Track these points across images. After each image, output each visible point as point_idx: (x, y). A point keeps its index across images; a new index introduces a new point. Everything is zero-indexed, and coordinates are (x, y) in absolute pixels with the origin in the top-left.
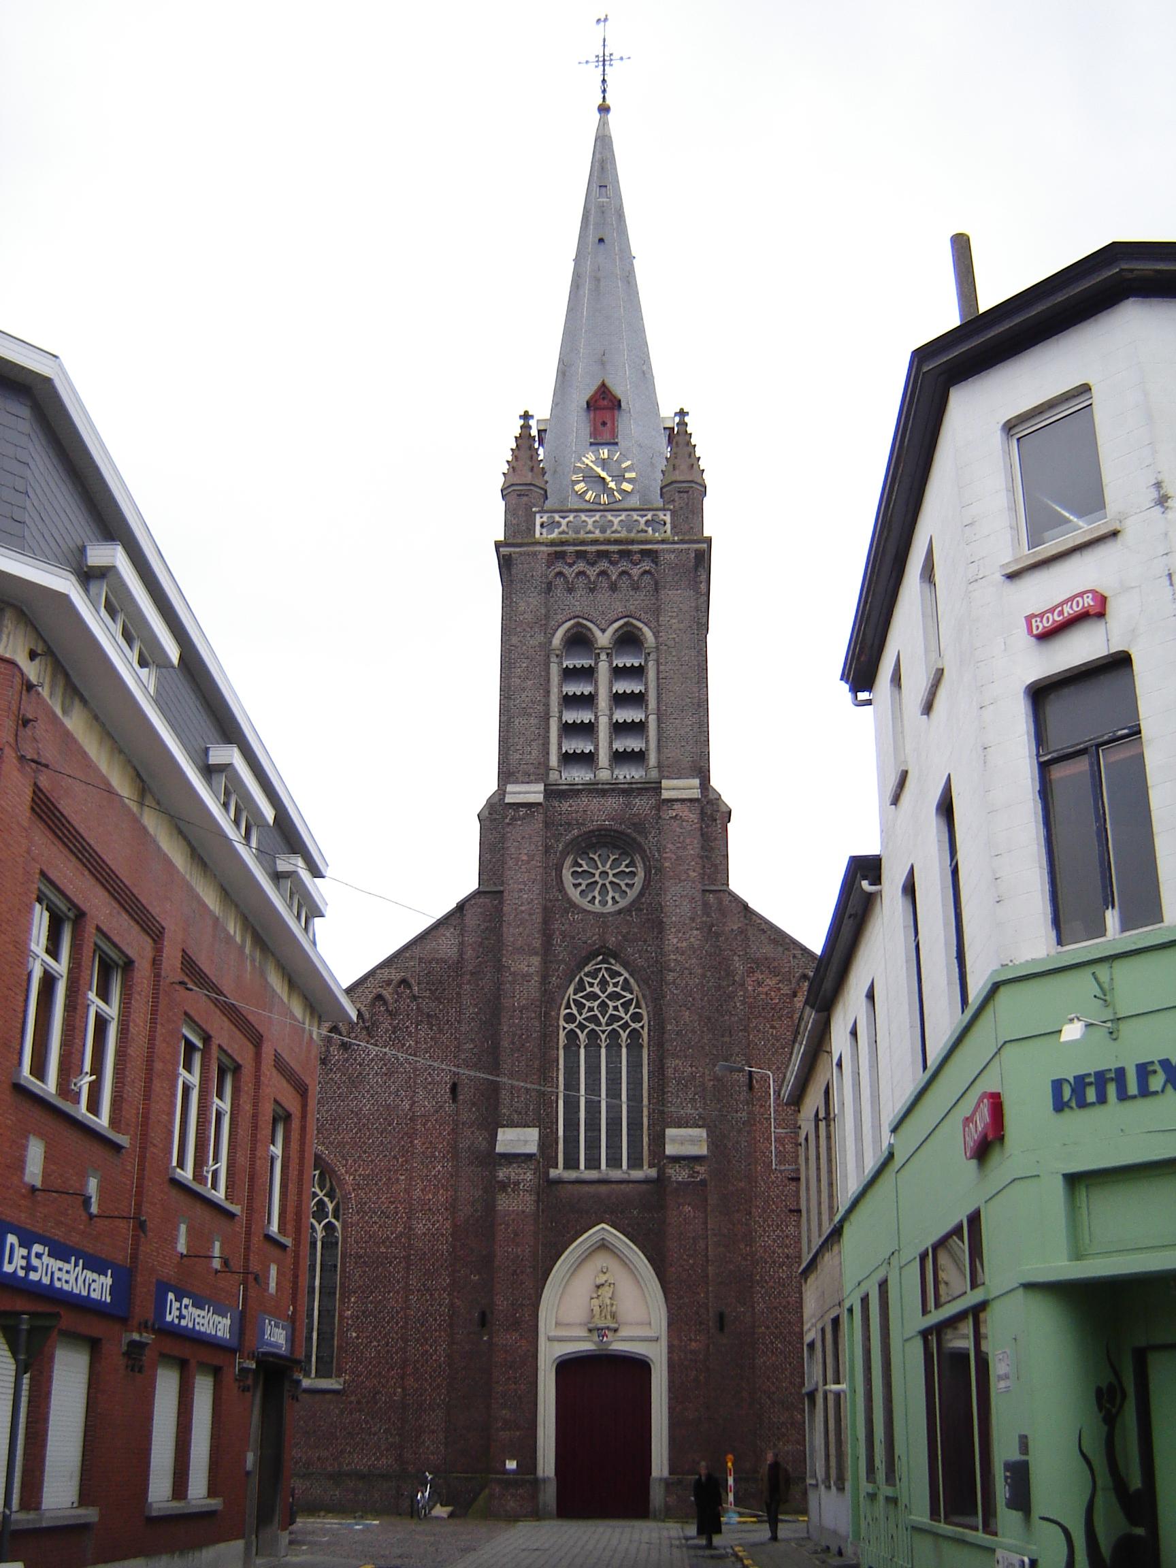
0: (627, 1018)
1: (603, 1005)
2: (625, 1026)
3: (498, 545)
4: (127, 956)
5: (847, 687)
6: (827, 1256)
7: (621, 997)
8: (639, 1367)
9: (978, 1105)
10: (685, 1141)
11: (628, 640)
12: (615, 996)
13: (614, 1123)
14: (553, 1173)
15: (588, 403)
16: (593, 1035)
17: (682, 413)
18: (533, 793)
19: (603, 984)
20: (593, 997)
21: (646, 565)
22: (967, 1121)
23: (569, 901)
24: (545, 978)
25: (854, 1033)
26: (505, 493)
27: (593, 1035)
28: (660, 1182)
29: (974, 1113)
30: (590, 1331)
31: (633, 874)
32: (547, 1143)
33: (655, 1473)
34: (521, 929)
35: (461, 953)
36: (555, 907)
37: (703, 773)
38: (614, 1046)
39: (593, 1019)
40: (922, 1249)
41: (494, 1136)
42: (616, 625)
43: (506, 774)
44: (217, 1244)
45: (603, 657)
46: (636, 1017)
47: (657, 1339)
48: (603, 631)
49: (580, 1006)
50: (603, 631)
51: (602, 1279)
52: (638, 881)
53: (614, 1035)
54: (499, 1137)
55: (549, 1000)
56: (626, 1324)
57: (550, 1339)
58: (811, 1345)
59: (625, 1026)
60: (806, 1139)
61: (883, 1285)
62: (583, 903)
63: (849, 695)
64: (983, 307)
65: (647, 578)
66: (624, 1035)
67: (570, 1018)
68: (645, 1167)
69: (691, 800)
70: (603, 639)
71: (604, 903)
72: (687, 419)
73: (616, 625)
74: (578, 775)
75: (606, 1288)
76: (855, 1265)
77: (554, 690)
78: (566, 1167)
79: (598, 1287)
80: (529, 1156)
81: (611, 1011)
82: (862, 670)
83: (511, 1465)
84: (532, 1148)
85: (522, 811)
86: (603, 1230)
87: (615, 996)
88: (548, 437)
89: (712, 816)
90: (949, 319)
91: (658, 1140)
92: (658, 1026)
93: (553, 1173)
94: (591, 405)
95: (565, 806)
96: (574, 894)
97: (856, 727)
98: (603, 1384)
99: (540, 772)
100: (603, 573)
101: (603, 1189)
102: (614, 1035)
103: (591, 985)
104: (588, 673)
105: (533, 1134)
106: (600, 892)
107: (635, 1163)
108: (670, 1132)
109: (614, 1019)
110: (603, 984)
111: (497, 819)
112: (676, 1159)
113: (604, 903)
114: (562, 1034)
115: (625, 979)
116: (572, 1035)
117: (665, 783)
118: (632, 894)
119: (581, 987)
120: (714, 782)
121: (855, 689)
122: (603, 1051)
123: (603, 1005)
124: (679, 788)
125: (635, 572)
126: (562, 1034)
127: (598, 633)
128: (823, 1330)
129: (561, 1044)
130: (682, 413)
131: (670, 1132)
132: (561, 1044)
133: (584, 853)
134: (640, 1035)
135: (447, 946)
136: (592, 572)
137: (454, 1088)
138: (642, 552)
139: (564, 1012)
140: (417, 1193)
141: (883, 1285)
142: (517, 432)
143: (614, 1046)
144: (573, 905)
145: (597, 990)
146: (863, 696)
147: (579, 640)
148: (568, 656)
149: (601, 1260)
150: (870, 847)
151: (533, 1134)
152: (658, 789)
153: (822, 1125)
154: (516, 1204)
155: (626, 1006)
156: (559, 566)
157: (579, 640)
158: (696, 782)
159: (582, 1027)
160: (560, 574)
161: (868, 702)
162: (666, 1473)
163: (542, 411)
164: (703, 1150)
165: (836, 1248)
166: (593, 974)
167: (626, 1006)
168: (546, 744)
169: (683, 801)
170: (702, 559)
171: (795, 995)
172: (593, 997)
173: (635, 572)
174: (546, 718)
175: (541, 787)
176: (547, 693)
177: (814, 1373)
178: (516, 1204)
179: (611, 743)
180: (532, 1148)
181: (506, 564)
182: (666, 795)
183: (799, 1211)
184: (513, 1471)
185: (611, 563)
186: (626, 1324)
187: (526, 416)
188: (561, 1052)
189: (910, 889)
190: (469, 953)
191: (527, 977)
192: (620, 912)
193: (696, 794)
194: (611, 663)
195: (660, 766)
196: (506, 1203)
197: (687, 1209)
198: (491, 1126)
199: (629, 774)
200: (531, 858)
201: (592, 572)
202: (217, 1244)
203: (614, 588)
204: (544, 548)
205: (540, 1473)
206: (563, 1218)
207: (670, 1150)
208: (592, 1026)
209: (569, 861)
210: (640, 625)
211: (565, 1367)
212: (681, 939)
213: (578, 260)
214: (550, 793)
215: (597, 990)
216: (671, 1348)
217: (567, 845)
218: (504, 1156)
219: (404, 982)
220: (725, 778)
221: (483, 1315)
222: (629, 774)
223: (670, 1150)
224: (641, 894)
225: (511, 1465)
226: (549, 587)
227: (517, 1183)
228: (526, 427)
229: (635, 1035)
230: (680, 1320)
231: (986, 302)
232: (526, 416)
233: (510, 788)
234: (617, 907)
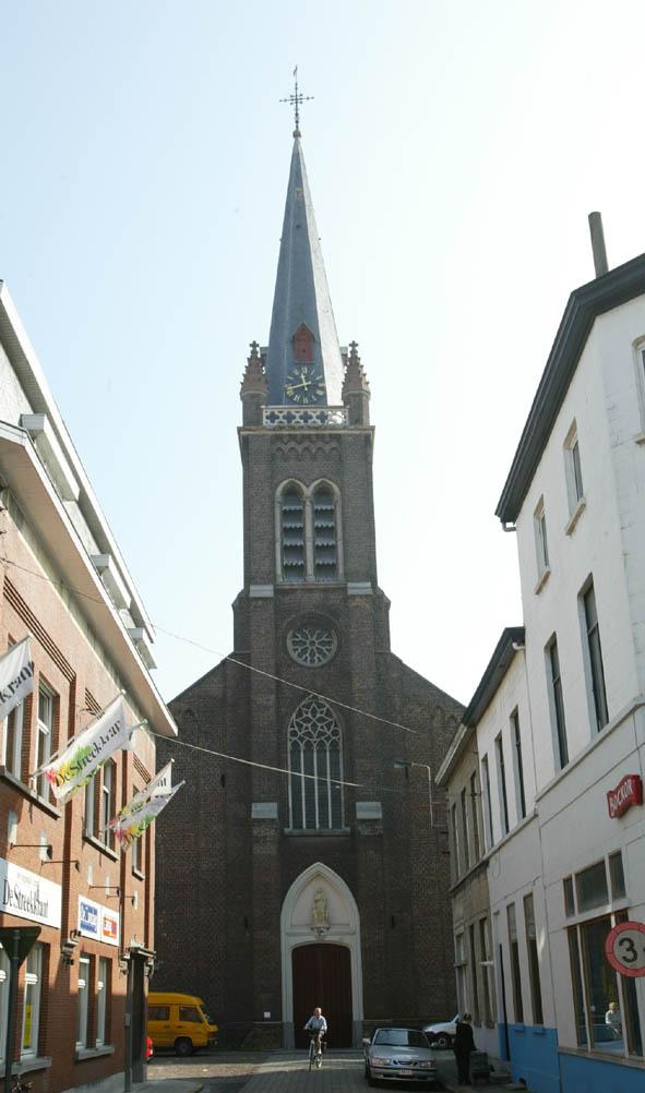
0: (329, 733)
1: (314, 726)
2: (328, 739)
3: (239, 430)
4: (56, 693)
5: (499, 519)
6: (475, 881)
7: (324, 720)
8: (342, 952)
9: (622, 784)
10: (368, 810)
11: (323, 493)
12: (321, 720)
13: (323, 799)
14: (287, 830)
15: (294, 337)
16: (309, 745)
17: (354, 345)
18: (266, 591)
19: (314, 712)
20: (307, 720)
21: (334, 444)
22: (611, 794)
23: (291, 659)
24: (278, 708)
25: (499, 740)
26: (242, 398)
27: (309, 745)
28: (353, 834)
29: (618, 788)
30: (312, 929)
31: (329, 643)
32: (283, 812)
33: (355, 1018)
34: (262, 673)
35: (224, 695)
36: (282, 665)
37: (373, 578)
38: (322, 751)
39: (309, 734)
40: (565, 876)
41: (249, 810)
42: (316, 483)
43: (249, 578)
44: (108, 879)
45: (308, 503)
46: (335, 733)
47: (354, 933)
48: (308, 486)
49: (300, 726)
50: (308, 486)
51: (319, 896)
52: (334, 647)
53: (321, 744)
54: (253, 808)
55: (281, 720)
56: (334, 924)
57: (288, 934)
58: (459, 936)
59: (328, 739)
60: (454, 807)
61: (528, 898)
62: (300, 661)
63: (501, 524)
64: (611, 268)
65: (334, 452)
66: (302, 745)
67: (294, 734)
68: (343, 826)
69: (366, 596)
70: (308, 491)
71: (312, 661)
72: (357, 348)
73: (316, 483)
74: (296, 582)
75: (320, 902)
76: (503, 885)
77: (339, 522)
78: (295, 827)
79: (316, 901)
80: (273, 820)
81: (319, 729)
82: (509, 510)
83: (267, 1015)
84: (274, 815)
85: (260, 603)
86: (319, 867)
87: (321, 720)
88: (267, 358)
89: (380, 604)
90: (589, 275)
91: (351, 810)
92: (349, 738)
93: (287, 830)
94: (294, 340)
95: (287, 599)
96: (294, 655)
97: (506, 548)
98: (322, 964)
99: (270, 578)
100: (307, 449)
101: (318, 839)
102: (321, 744)
103: (307, 713)
104: (299, 514)
105: (274, 806)
106: (309, 653)
107: (337, 823)
108: (358, 804)
109: (321, 734)
110: (314, 712)
111: (244, 608)
112: (363, 821)
113: (312, 661)
114: (289, 744)
115: (328, 710)
116: (295, 744)
117: (350, 585)
118: (330, 656)
119: (300, 714)
120: (379, 585)
121: (504, 521)
122: (315, 754)
123: (314, 726)
124: (358, 588)
125: (327, 448)
126: (289, 744)
127: (304, 487)
128: (472, 927)
129: (289, 750)
130: (354, 345)
131: (358, 804)
132: (289, 750)
133: (299, 630)
134: (338, 744)
135: (215, 689)
136: (300, 449)
137: (223, 779)
138: (330, 435)
139: (290, 729)
140: (203, 845)
141: (528, 898)
142: (249, 355)
143: (322, 751)
144: (293, 661)
145: (310, 716)
146: (510, 525)
147: (292, 493)
148: (317, 503)
149: (317, 884)
150: (518, 623)
151: (274, 806)
152: (345, 589)
153: (468, 800)
154: (266, 850)
155: (328, 726)
156: (279, 445)
157: (292, 493)
158: (369, 584)
159: (301, 739)
160: (280, 449)
161: (513, 529)
162: (362, 1018)
163: (264, 342)
164: (379, 815)
165: (482, 876)
166: (308, 706)
167: (328, 726)
168: (274, 560)
169: (361, 596)
170: (367, 441)
171: (433, 717)
172: (307, 720)
173: (327, 448)
174: (273, 543)
175: (271, 587)
176: (274, 527)
177: (462, 954)
178: (266, 850)
179: (314, 561)
180: (274, 815)
181: (245, 443)
182: (350, 592)
183: (449, 853)
184: (267, 1019)
185: (312, 442)
186: (334, 924)
187: (254, 345)
188: (289, 755)
189: (552, 648)
190: (230, 693)
191: (267, 708)
192: (323, 666)
193: (370, 592)
194: (313, 508)
195: (346, 574)
196: (258, 850)
197: (371, 852)
198: (248, 800)
199: (326, 581)
200: (268, 632)
201: (300, 449)
202: (108, 879)
203: (314, 458)
204: (270, 433)
205: (284, 1020)
206: (293, 862)
207: (360, 815)
208: (307, 738)
209: (290, 635)
210: (331, 483)
211: (298, 952)
212: (363, 682)
213: (284, 240)
214: (277, 591)
215: (310, 716)
216: (363, 940)
217: (288, 624)
218: (256, 820)
219: (189, 711)
220: (383, 583)
221: (246, 920)
222: (326, 581)
223: (360, 815)
224: (336, 655)
225: (267, 1015)
226: (273, 457)
227: (265, 837)
228: (254, 352)
229: (334, 745)
230: (366, 923)
231: (615, 261)
232: (254, 345)
233: (252, 588)
234: (320, 664)
